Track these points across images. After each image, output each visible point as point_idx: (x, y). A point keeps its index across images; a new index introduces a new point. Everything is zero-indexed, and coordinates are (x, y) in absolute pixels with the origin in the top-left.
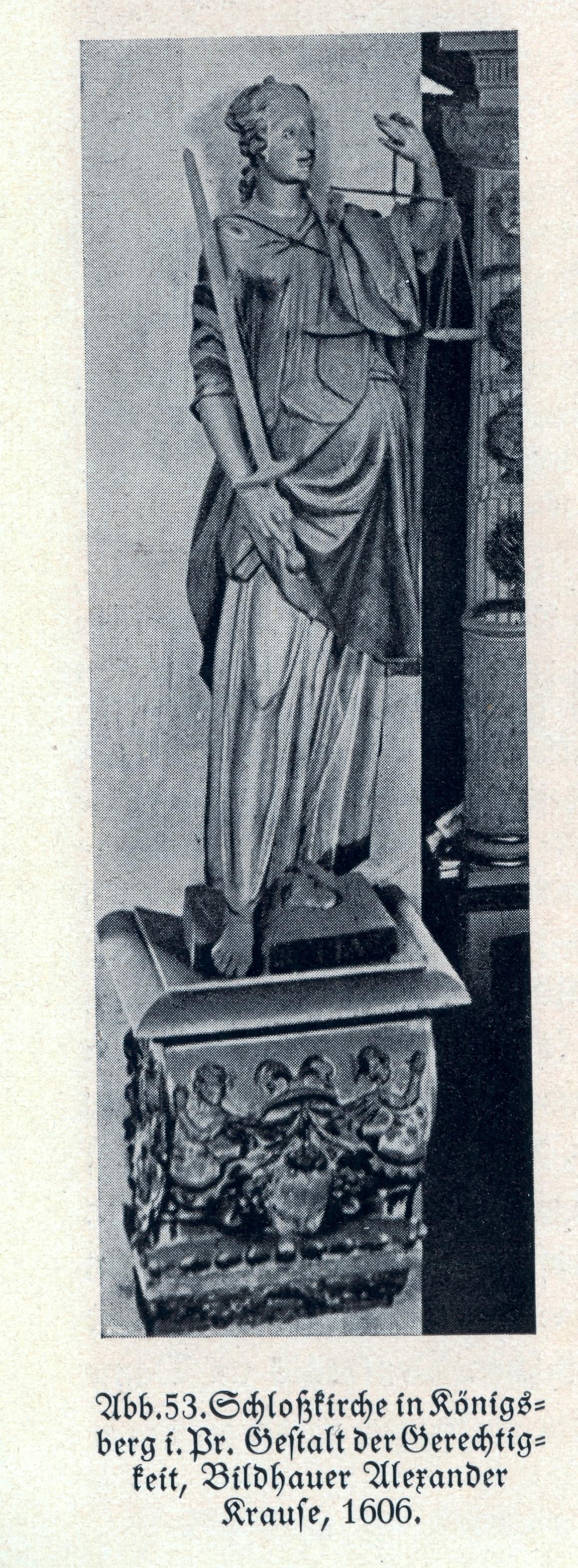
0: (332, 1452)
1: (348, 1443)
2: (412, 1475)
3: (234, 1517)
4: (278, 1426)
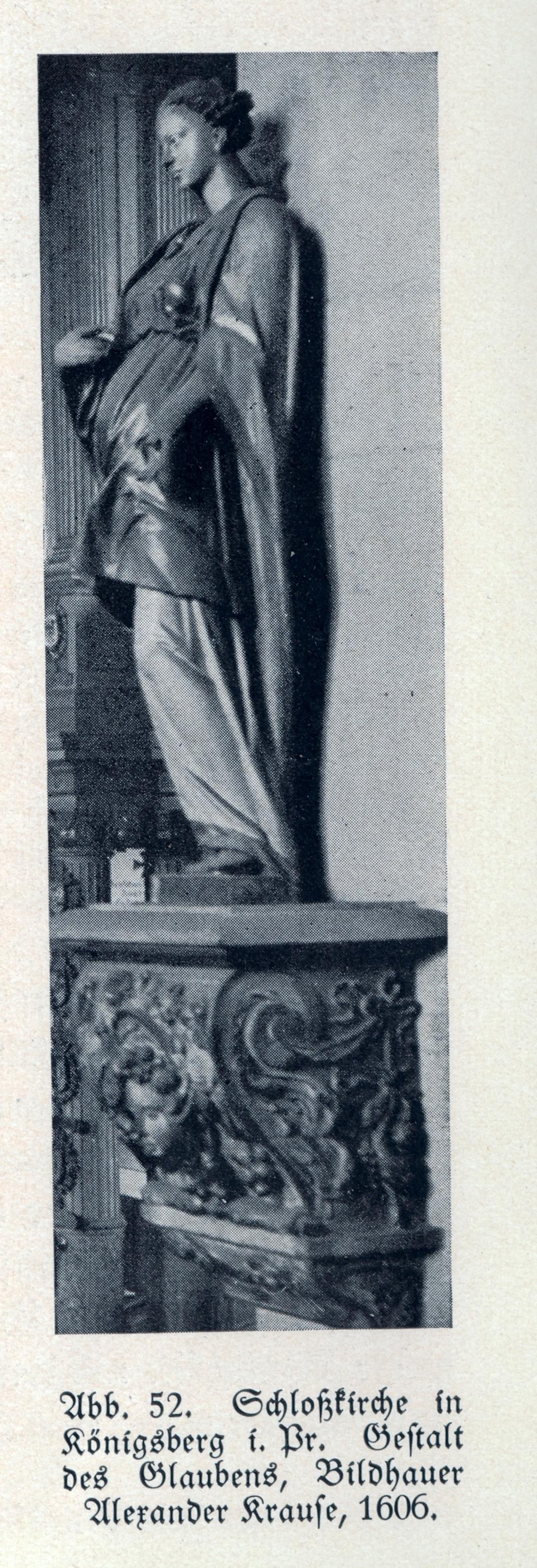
0: (451, 1447)
2: (132, 1511)
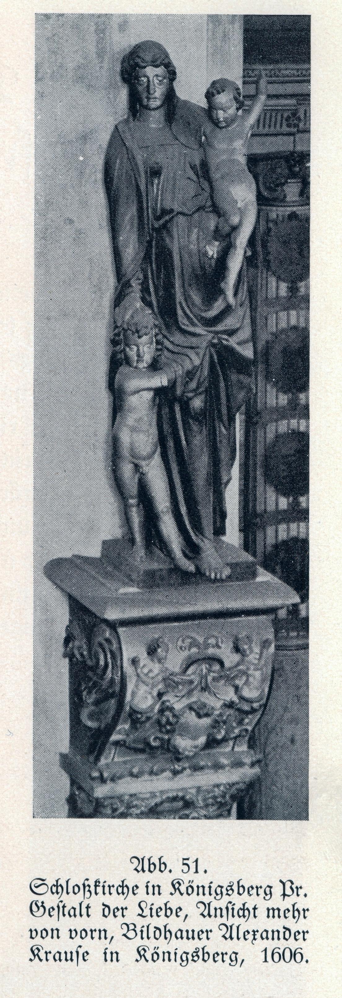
2: (248, 932)
3: (36, 957)
4: (72, 901)
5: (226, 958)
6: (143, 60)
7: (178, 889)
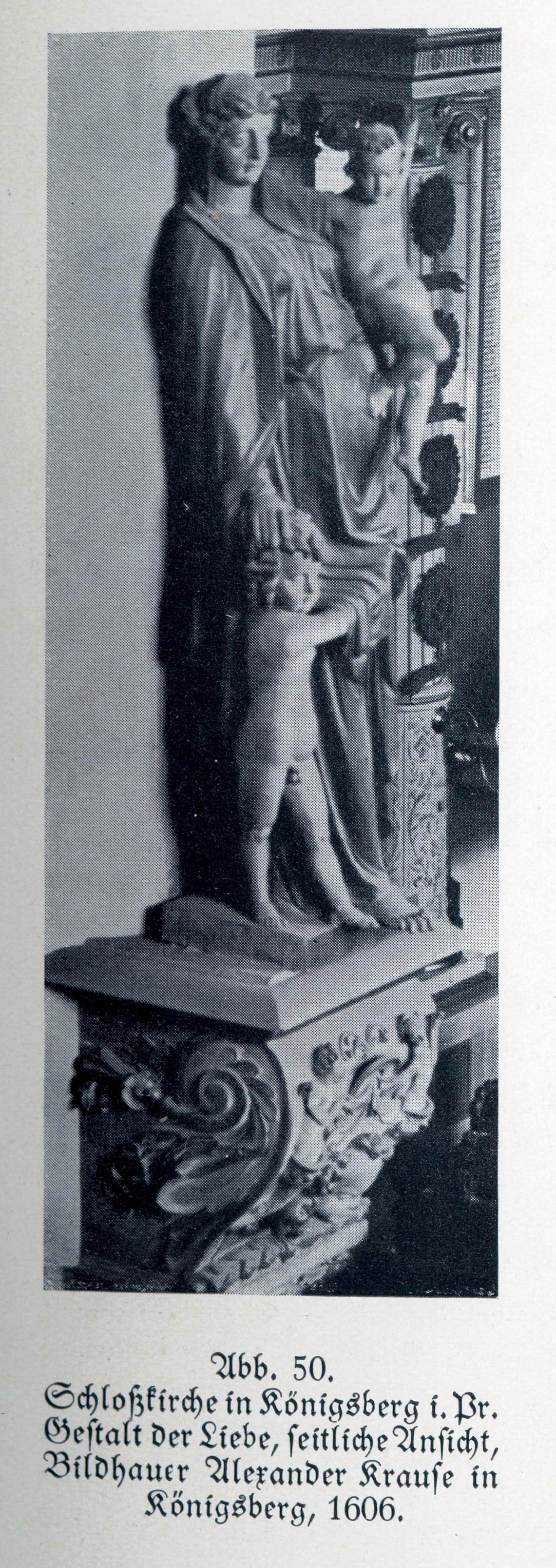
1: (146, 1436)
4: (110, 1419)
5: (287, 1512)
6: (249, 105)
7: (273, 1404)
